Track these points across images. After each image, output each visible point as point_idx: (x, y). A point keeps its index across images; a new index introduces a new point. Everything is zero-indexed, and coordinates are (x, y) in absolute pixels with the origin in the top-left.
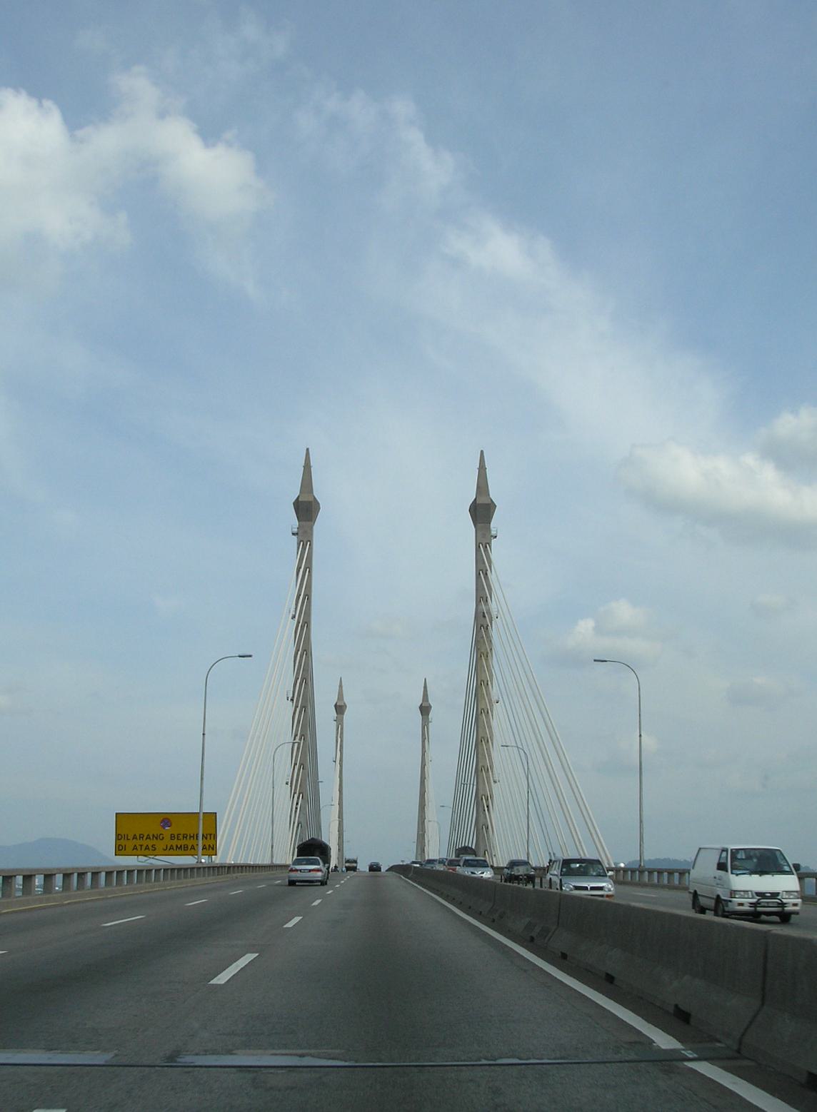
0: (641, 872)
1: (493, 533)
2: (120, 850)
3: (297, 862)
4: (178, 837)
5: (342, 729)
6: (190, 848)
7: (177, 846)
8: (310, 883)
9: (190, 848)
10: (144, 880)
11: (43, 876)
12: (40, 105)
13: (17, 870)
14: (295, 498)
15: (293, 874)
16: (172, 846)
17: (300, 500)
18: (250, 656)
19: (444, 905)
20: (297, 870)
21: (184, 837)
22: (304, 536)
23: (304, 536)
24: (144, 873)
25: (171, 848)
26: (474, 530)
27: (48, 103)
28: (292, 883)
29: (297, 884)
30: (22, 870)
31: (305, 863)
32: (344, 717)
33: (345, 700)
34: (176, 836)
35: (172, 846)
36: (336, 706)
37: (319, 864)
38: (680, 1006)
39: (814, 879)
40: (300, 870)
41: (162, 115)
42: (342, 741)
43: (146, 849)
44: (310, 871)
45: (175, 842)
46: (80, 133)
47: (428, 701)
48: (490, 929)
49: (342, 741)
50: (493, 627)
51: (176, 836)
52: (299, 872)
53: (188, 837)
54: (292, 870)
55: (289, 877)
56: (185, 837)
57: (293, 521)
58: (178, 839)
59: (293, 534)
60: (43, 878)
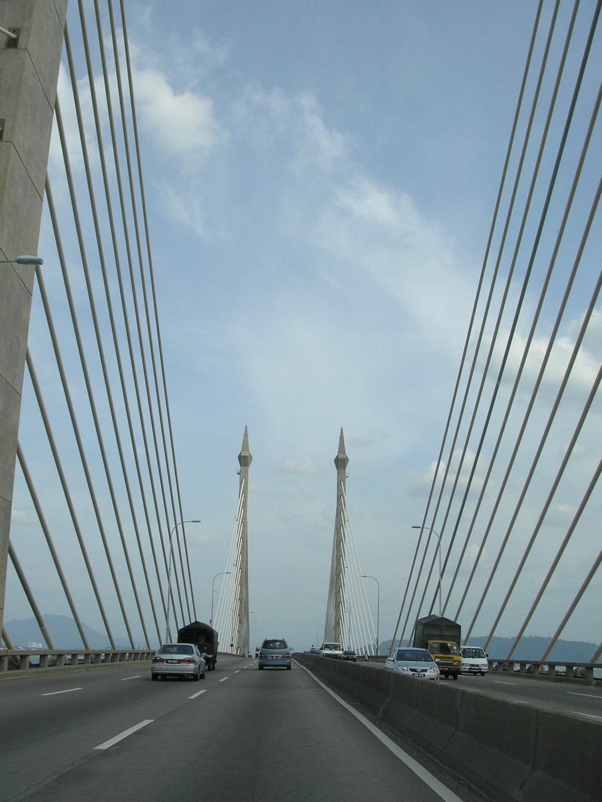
1: (347, 475)
2: (178, 642)
5: (246, 483)
8: (181, 678)
11: (39, 656)
13: (101, 651)
18: (200, 522)
19: (310, 676)
20: (162, 660)
22: (243, 475)
23: (243, 475)
28: (155, 677)
33: (250, 450)
36: (240, 457)
39: (565, 667)
40: (167, 661)
44: (180, 661)
54: (155, 661)
55: (152, 669)
60: (39, 658)
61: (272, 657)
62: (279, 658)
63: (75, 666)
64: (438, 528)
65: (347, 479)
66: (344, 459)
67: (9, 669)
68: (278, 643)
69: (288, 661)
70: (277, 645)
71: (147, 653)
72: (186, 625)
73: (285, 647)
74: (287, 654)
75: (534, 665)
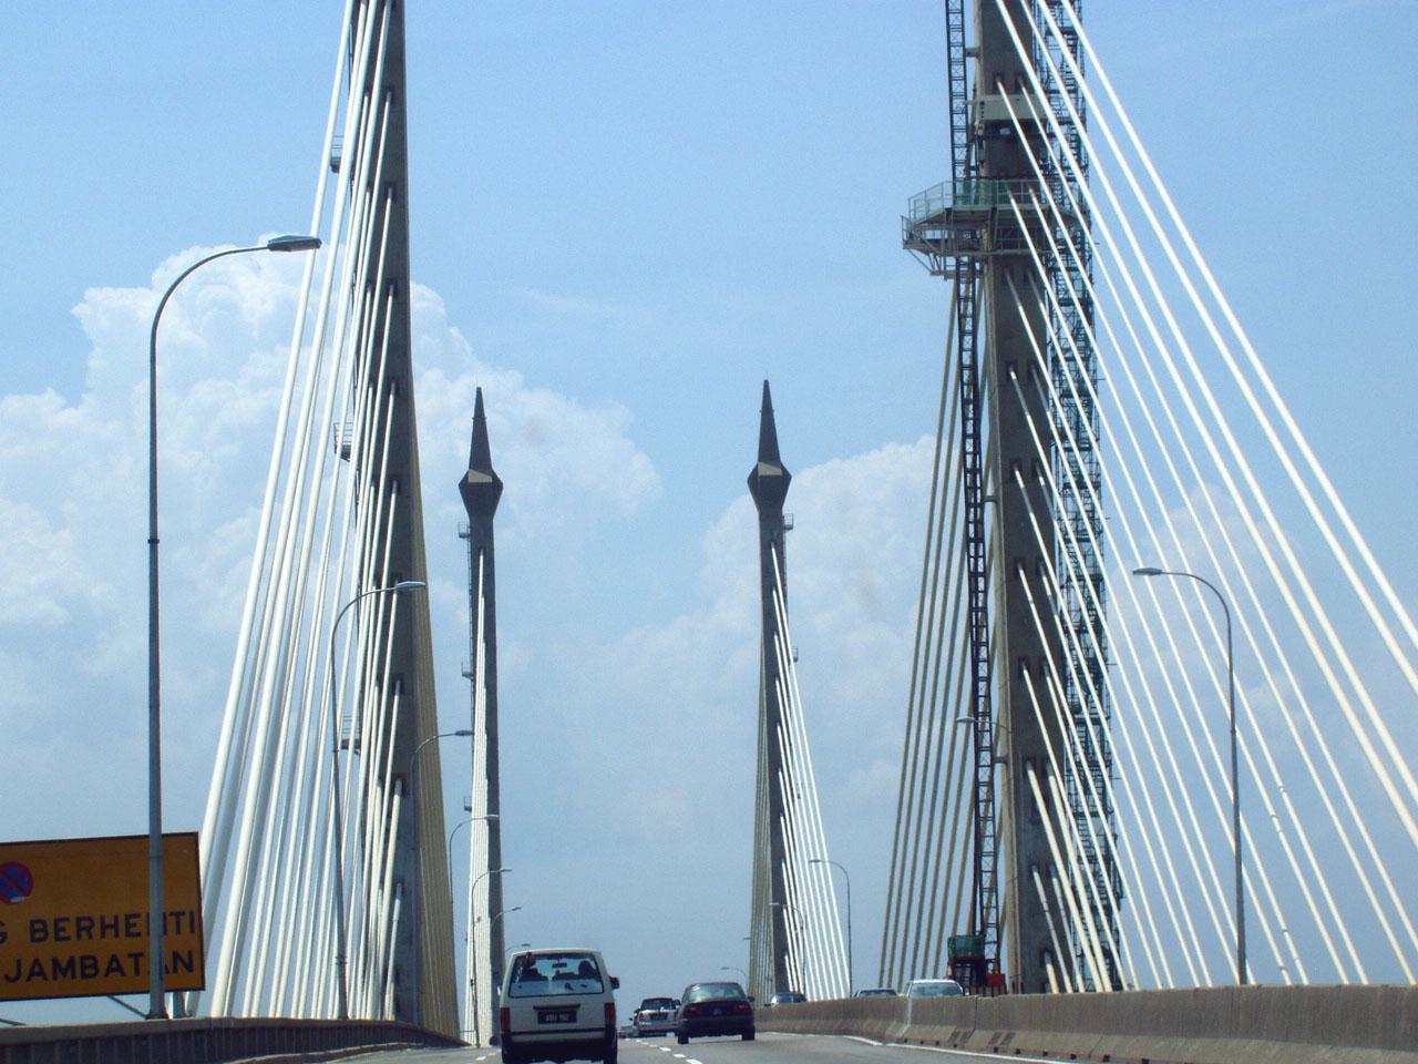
1: (787, 522)
4: (57, 930)
6: (103, 966)
7: (56, 963)
9: (103, 966)
16: (36, 962)
21: (79, 929)
25: (37, 970)
34: (51, 930)
35: (36, 962)
38: (147, 290)
43: (110, 970)
45: (48, 951)
51: (51, 930)
53: (96, 930)
56: (84, 926)
58: (57, 938)
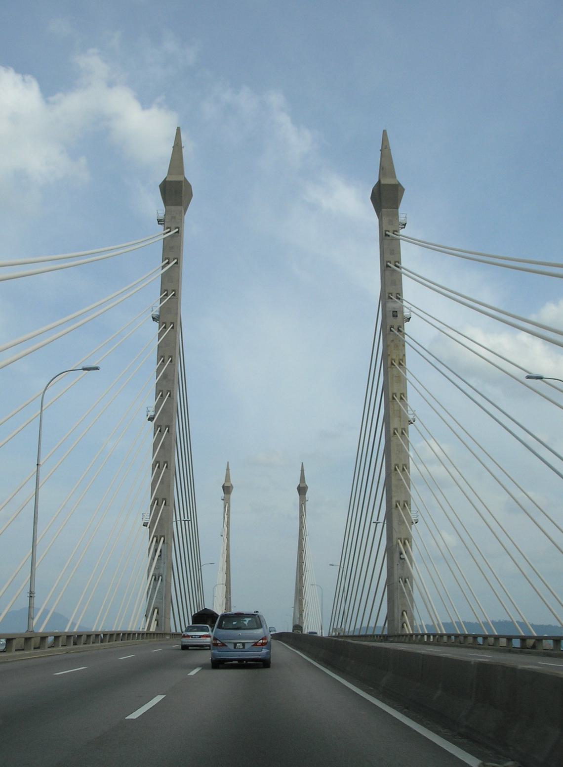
0: (374, 636)
1: (307, 499)
3: (189, 629)
5: (229, 507)
10: (131, 639)
12: (24, 80)
14: (163, 180)
15: (185, 640)
17: (225, 485)
20: (188, 636)
22: (226, 500)
23: (226, 500)
24: (126, 635)
26: (377, 220)
27: (28, 78)
28: (185, 647)
29: (190, 648)
30: (4, 634)
31: (195, 630)
32: (231, 496)
36: (224, 487)
37: (208, 631)
39: (519, 640)
41: (111, 84)
42: (228, 518)
44: (200, 636)
46: (52, 99)
47: (305, 482)
48: (369, 696)
49: (228, 518)
50: (307, 517)
52: (190, 638)
54: (184, 636)
57: (221, 493)
59: (222, 500)
61: (235, 644)
62: (247, 646)
63: (89, 645)
64: (345, 569)
65: (307, 502)
66: (304, 487)
67: (74, 645)
68: (248, 620)
69: (264, 651)
70: (246, 623)
71: (138, 634)
72: (355, 634)
73: (260, 626)
74: (262, 639)
75: (536, 640)
